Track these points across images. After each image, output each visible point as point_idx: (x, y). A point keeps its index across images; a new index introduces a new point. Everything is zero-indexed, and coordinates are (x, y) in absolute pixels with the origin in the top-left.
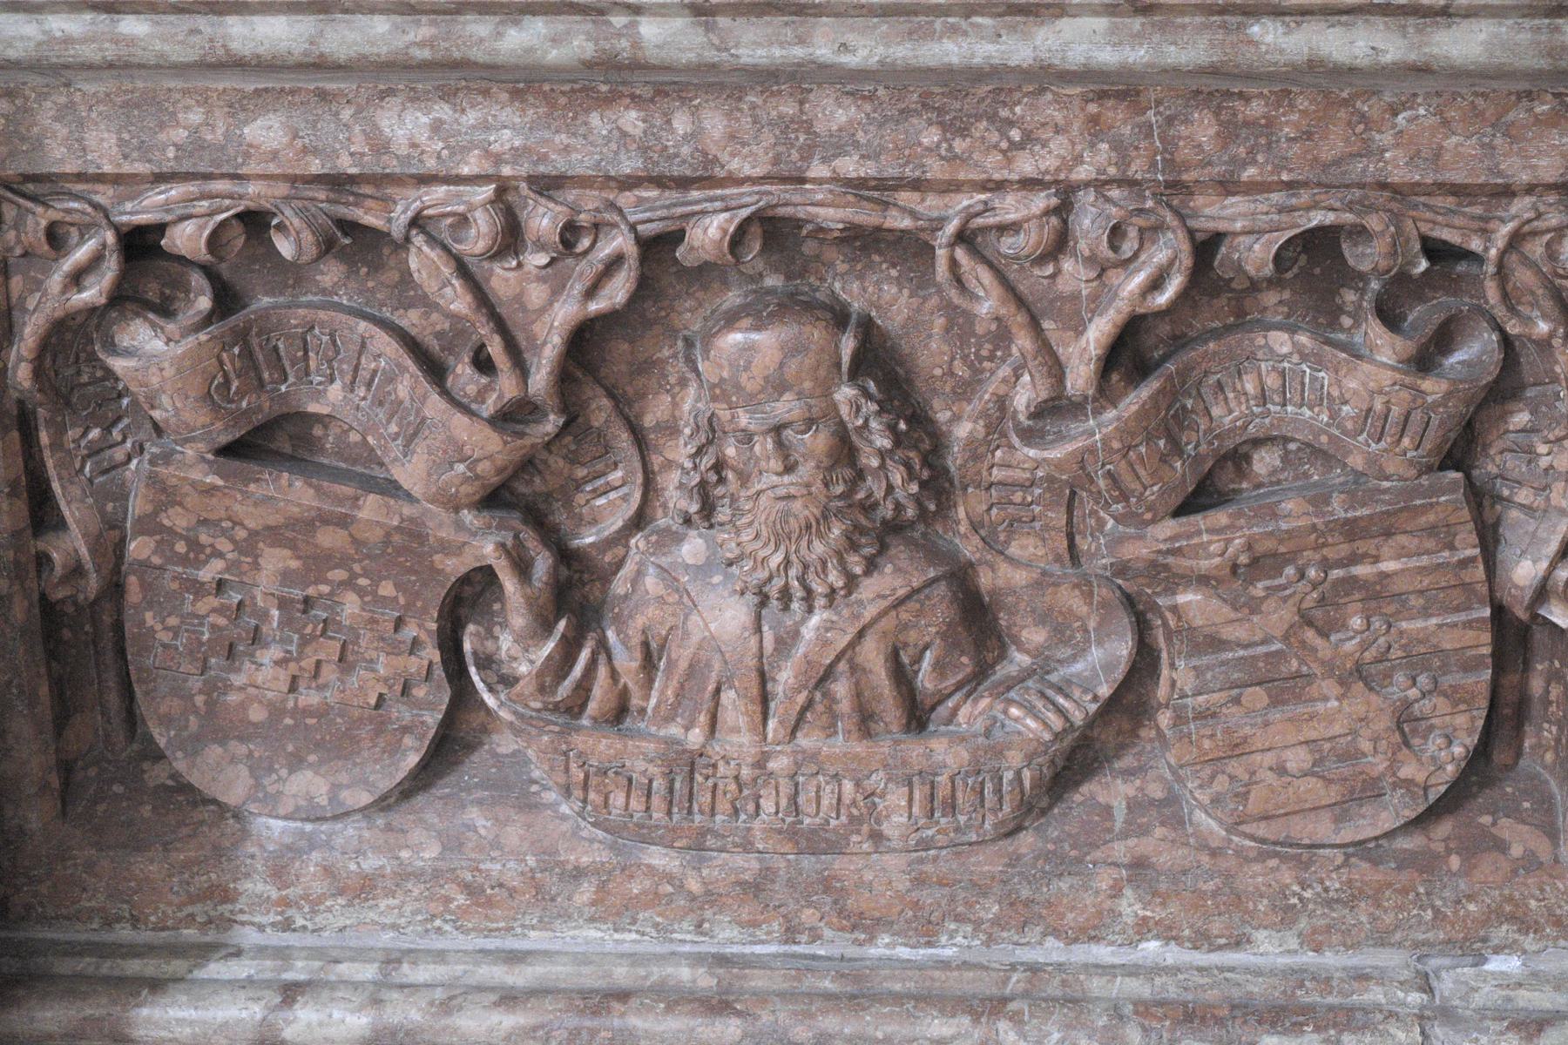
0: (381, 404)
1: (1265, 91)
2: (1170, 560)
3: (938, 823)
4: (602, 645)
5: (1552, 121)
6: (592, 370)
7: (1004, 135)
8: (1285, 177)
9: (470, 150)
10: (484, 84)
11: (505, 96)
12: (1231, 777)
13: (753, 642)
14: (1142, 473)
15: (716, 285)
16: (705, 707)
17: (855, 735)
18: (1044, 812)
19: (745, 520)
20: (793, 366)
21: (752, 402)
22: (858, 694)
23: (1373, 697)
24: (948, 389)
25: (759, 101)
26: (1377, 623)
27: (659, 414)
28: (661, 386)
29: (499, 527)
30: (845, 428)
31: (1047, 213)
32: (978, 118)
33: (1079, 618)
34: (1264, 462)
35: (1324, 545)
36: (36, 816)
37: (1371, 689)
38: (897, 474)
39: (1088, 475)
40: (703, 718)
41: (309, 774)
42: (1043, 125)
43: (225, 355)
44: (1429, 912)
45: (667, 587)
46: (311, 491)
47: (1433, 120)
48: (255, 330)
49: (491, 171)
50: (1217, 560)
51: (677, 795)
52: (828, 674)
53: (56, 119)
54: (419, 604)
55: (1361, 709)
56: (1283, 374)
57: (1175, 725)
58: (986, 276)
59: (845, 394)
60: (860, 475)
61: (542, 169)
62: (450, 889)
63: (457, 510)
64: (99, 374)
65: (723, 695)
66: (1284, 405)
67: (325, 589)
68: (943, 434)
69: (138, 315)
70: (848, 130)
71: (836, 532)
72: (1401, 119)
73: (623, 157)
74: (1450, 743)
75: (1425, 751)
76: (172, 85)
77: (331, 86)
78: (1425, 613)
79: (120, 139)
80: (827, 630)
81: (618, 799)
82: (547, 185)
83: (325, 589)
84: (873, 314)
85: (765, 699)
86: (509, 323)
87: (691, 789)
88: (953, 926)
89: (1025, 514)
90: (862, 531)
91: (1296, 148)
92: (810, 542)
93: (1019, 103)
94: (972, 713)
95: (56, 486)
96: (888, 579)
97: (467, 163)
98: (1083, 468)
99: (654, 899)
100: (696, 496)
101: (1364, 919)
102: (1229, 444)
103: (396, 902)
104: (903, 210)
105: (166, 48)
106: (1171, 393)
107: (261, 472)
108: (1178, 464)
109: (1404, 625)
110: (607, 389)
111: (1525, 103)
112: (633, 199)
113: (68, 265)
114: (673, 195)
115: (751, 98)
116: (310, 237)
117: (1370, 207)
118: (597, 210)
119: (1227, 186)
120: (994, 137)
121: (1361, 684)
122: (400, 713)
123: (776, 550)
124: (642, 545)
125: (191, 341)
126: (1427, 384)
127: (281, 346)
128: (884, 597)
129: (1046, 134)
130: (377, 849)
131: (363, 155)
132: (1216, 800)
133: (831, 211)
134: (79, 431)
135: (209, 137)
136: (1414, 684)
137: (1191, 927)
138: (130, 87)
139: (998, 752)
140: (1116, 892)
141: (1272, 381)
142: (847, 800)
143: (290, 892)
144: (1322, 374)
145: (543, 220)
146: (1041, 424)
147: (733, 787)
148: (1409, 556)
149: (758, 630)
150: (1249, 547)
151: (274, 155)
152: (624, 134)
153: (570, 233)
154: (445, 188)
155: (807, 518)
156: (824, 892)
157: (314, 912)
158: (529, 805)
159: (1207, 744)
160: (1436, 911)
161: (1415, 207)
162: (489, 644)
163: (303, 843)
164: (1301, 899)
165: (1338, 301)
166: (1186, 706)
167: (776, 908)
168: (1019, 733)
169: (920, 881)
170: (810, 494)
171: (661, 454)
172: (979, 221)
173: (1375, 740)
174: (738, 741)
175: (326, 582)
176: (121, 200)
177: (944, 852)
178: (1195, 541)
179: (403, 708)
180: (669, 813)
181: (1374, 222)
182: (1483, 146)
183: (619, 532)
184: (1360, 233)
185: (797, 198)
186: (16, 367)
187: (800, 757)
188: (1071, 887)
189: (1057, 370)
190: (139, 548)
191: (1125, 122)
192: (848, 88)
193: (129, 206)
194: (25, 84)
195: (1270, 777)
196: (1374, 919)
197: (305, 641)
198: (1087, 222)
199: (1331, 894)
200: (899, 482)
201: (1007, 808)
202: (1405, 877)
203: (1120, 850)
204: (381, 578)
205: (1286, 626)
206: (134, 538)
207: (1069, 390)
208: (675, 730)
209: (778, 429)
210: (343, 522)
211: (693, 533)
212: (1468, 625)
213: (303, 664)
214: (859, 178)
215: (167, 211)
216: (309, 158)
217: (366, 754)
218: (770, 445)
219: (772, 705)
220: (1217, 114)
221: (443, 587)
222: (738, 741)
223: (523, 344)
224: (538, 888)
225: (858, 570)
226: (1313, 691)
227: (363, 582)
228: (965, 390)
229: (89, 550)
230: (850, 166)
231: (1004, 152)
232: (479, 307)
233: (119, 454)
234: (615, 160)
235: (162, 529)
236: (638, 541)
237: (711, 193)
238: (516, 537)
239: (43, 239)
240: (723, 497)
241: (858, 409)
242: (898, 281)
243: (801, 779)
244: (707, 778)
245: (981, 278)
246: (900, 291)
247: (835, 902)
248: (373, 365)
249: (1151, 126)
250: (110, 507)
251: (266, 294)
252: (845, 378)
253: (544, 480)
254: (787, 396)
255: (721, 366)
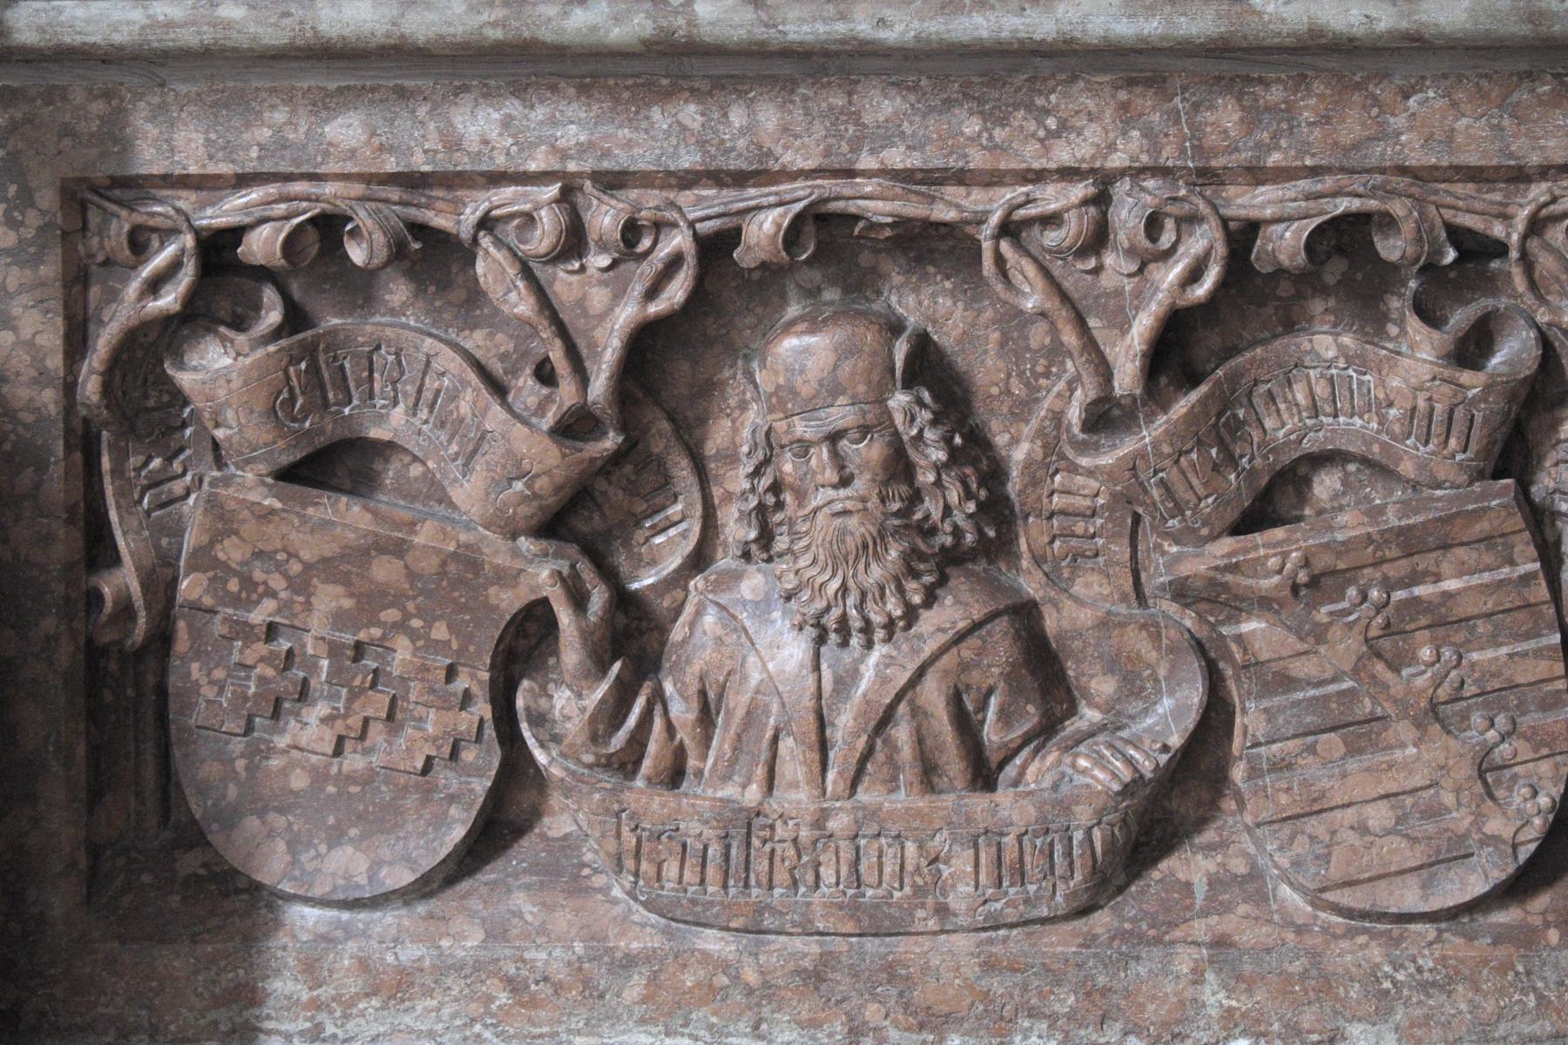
0: (443, 424)
1: (1283, 76)
2: (1229, 578)
3: (1006, 893)
4: (658, 696)
5: (1554, 101)
6: (652, 393)
7: (1041, 123)
8: (1308, 162)
9: (537, 145)
10: (553, 80)
11: (572, 91)
12: (1312, 838)
13: (811, 681)
14: (1195, 482)
15: (775, 300)
16: (763, 757)
17: (917, 787)
18: (1120, 890)
19: (802, 543)
20: (847, 367)
21: (809, 409)
22: (920, 741)
23: (1452, 742)
24: (1005, 410)
25: (811, 94)
26: (1447, 653)
27: (719, 441)
28: (721, 410)
29: (557, 555)
30: (901, 440)
31: (1085, 202)
32: (1016, 107)
33: (1149, 666)
34: (1325, 484)
35: (1384, 561)
36: (59, 901)
37: (1449, 732)
38: (958, 520)
39: (1141, 484)
40: (760, 772)
41: (349, 850)
42: (1077, 112)
43: (291, 369)
44: (1532, 996)
45: (724, 626)
46: (369, 516)
47: (1442, 103)
48: (322, 346)
49: (557, 167)
50: (1276, 579)
51: (733, 863)
52: (887, 718)
53: (147, 120)
54: (472, 648)
55: (1441, 757)
56: (1331, 380)
57: (1249, 778)
58: (1030, 269)
59: (899, 400)
60: (916, 497)
61: (606, 165)
62: (493, 985)
63: (514, 537)
64: (165, 398)
65: (781, 744)
66: (1336, 416)
67: (376, 632)
68: (1002, 458)
69: (208, 330)
70: (896, 119)
71: (894, 553)
72: (1412, 102)
73: (682, 151)
74: (1535, 793)
75: (1510, 804)
76: (260, 84)
77: (409, 83)
78: (1494, 641)
79: (207, 140)
80: (887, 666)
81: (671, 869)
82: (612, 182)
83: (376, 632)
84: (929, 329)
85: (823, 746)
86: (571, 331)
87: (748, 855)
88: (1026, 1024)
89: (1087, 546)
90: (922, 557)
91: (1317, 132)
92: (867, 565)
93: (1054, 91)
94: (1039, 770)
95: (113, 516)
96: (949, 611)
97: (534, 159)
98: (1135, 476)
99: (709, 993)
100: (754, 521)
101: (1463, 1006)
102: (1286, 458)
103: (435, 1002)
104: (950, 204)
105: (260, 30)
106: (1224, 401)
107: (319, 497)
108: (1233, 477)
109: (1475, 656)
110: (668, 413)
111: (1526, 84)
112: (693, 198)
113: (147, 271)
114: (729, 194)
115: (802, 90)
116: (382, 238)
117: (1391, 192)
118: (657, 208)
119: (1257, 175)
120: (1031, 126)
121: (1438, 726)
122: (447, 778)
123: (834, 575)
124: (701, 585)
125: (260, 353)
126: (1466, 377)
127: (347, 365)
128: (944, 631)
129: (1081, 122)
130: (416, 939)
131: (436, 152)
132: (1297, 864)
133: (880, 204)
134: (141, 459)
135: (291, 136)
136: (1492, 725)
137: (1280, 1019)
138: (221, 87)
139: (1065, 807)
140: (1198, 979)
141: (1321, 390)
142: (909, 867)
143: (325, 992)
144: (1368, 377)
145: (605, 218)
146: (1095, 438)
147: (792, 852)
148: (1472, 572)
149: (817, 668)
150: (1306, 563)
151: (353, 152)
152: (684, 128)
153: (631, 231)
154: (513, 188)
155: (863, 536)
156: (889, 982)
157: (346, 1017)
158: (578, 888)
159: (1284, 799)
160: (1540, 997)
161: (1436, 192)
162: (543, 702)
163: (339, 933)
164: (1394, 983)
165: (1382, 307)
166: (1259, 756)
167: (838, 1002)
168: (1088, 786)
169: (990, 966)
170: (865, 509)
171: (721, 485)
172: (1022, 213)
173: (1458, 791)
174: (796, 796)
175: (378, 624)
176: (203, 206)
177: (1015, 932)
178: (1252, 555)
179: (450, 774)
180: (725, 886)
181: (1398, 208)
182: (1492, 127)
183: (677, 571)
184: (1388, 222)
185: (847, 192)
186: (85, 381)
187: (860, 814)
188: (1150, 971)
189: (1105, 371)
190: (189, 586)
191: (1154, 109)
192: (893, 79)
193: (209, 212)
194: (121, 84)
195: (1351, 838)
196: (1474, 1007)
197: (353, 696)
198: (1124, 213)
199: (1426, 975)
200: (956, 499)
201: (1078, 876)
202: (1502, 952)
203: (1200, 928)
204: (435, 619)
205: (1354, 658)
206: (186, 575)
207: (1118, 392)
208: (729, 791)
209: (834, 438)
210: (398, 549)
211: (752, 568)
212: (1538, 653)
213: (349, 721)
214: (906, 170)
215: (247, 214)
216: (385, 156)
217: (410, 827)
218: (825, 454)
219: (832, 755)
220: (1239, 100)
221: (497, 627)
222: (796, 796)
223: (584, 352)
224: (586, 983)
225: (917, 599)
226: (1389, 736)
227: (416, 623)
228: (1022, 409)
229: (143, 584)
230: (897, 157)
231: (1041, 141)
232: (541, 311)
233: (177, 487)
234: (675, 155)
235: (215, 564)
236: (697, 583)
237: (767, 190)
238: (573, 566)
239: (125, 244)
240: (781, 524)
241: (913, 419)
242: (952, 294)
243: (863, 842)
244: (765, 842)
245: (1024, 271)
246: (955, 303)
247: (901, 995)
248: (436, 385)
249: (1178, 112)
250: (165, 541)
251: (335, 316)
252: (899, 384)
253: (603, 515)
254: (842, 400)
255: (776, 373)
